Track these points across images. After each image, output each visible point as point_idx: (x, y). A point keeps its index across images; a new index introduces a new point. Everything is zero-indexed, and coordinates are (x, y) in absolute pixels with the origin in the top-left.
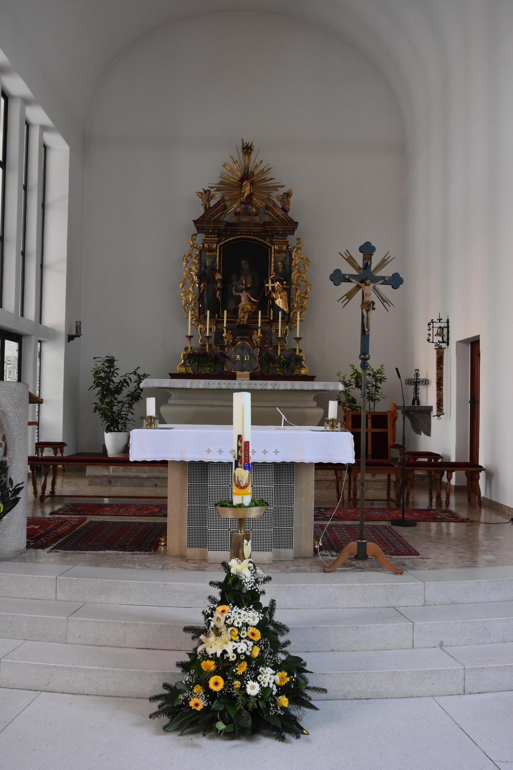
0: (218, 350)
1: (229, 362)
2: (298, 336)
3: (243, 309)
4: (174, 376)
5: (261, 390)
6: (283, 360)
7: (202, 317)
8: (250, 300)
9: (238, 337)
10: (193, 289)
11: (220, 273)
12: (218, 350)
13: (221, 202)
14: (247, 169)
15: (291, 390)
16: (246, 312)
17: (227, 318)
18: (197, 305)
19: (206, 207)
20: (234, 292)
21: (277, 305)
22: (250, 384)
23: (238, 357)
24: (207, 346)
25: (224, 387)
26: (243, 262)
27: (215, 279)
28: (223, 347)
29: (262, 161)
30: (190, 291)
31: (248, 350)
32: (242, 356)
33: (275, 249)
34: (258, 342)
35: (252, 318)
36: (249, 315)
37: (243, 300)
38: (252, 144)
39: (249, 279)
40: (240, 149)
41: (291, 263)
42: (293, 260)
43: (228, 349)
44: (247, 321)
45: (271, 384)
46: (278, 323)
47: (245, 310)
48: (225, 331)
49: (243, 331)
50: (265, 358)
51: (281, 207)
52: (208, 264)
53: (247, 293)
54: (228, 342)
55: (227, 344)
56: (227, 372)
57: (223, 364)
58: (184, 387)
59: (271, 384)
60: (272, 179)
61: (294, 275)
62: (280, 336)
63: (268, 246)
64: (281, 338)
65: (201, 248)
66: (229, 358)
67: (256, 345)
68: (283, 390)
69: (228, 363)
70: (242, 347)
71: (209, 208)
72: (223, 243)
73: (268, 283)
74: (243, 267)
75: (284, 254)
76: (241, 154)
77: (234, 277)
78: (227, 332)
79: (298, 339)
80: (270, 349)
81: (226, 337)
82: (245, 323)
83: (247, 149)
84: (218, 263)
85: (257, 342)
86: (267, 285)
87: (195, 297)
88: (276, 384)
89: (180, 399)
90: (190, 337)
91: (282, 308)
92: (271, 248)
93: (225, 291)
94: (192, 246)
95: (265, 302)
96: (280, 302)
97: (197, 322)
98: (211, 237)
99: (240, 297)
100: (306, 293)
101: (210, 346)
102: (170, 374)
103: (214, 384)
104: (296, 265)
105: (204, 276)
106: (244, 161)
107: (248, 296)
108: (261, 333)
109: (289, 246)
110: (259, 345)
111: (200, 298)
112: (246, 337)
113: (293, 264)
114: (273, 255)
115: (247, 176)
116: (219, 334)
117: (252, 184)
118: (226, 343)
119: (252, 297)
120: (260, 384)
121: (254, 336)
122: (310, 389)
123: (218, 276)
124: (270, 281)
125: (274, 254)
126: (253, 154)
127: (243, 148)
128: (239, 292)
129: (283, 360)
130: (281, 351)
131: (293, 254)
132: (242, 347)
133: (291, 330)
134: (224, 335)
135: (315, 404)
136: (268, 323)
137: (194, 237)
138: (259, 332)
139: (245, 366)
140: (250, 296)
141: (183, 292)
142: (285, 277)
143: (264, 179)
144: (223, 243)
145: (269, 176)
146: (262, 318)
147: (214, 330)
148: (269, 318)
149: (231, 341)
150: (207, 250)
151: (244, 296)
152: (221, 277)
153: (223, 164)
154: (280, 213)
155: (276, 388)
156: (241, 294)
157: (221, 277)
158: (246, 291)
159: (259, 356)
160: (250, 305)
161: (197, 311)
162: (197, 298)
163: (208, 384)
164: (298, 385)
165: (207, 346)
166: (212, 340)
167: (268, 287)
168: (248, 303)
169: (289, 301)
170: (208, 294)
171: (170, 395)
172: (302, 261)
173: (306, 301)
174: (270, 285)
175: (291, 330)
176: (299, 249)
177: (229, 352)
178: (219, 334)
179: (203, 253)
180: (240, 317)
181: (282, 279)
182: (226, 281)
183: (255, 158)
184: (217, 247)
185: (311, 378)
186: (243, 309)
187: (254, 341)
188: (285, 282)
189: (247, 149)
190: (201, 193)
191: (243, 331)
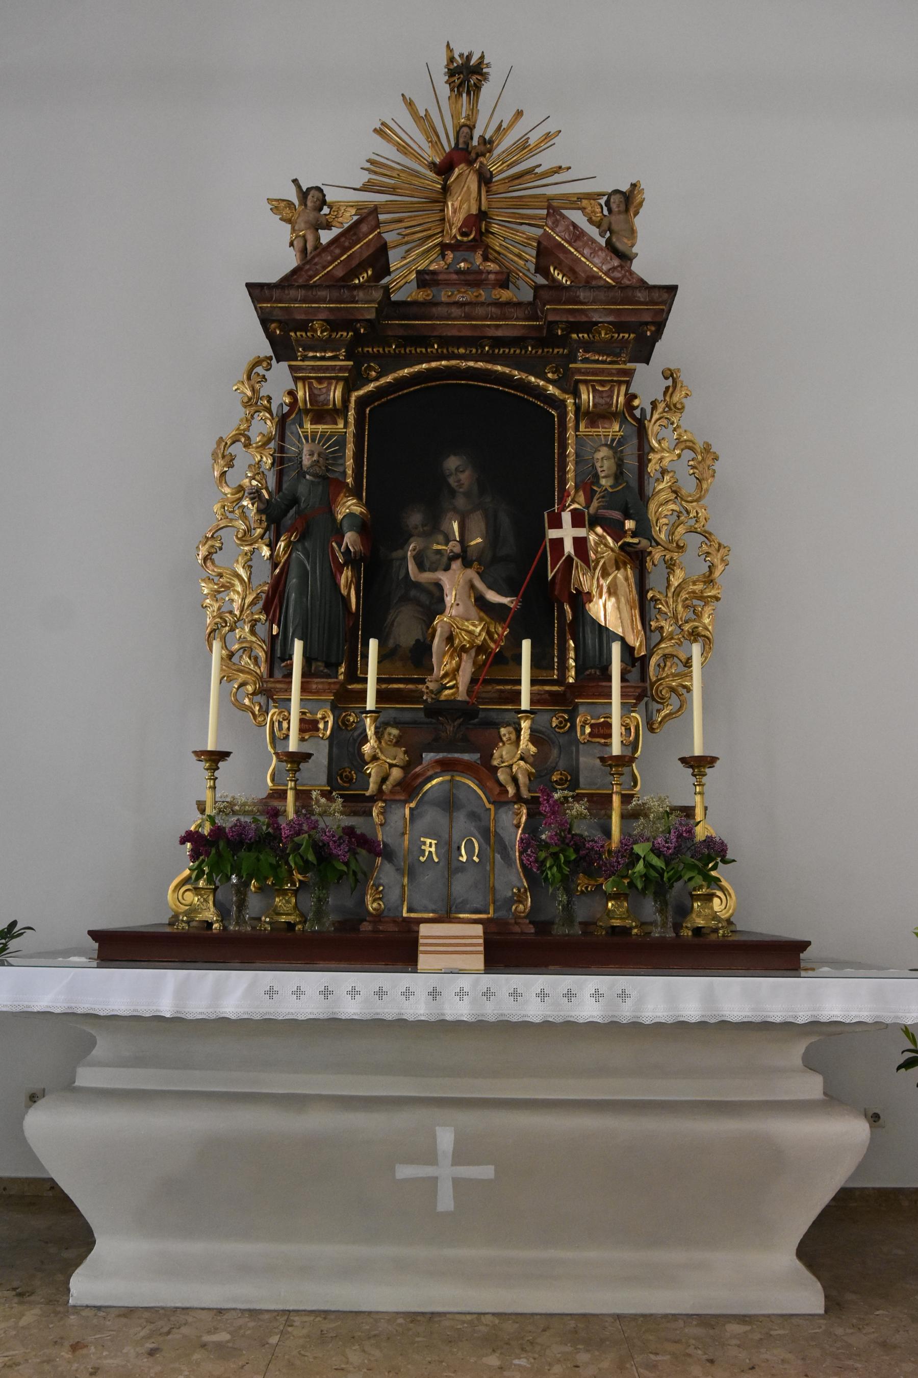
0: (334, 817)
1: (388, 867)
2: (698, 751)
3: (450, 639)
4: (118, 947)
5: (547, 1025)
6: (648, 865)
7: (278, 675)
8: (481, 603)
9: (429, 757)
10: (248, 567)
11: (356, 492)
12: (334, 817)
13: (364, 228)
14: (465, 130)
15: (702, 1025)
16: (463, 649)
17: (379, 681)
18: (261, 629)
19: (304, 250)
20: (412, 567)
21: (594, 622)
22: (488, 994)
23: (430, 846)
24: (290, 795)
25: (351, 1009)
26: (452, 463)
27: (334, 519)
28: (358, 803)
29: (519, 114)
30: (238, 576)
31: (473, 816)
32: (449, 843)
33: (577, 407)
34: (522, 779)
35: (486, 682)
36: (478, 667)
37: (450, 599)
38: (482, 57)
39: (477, 523)
40: (441, 78)
41: (643, 462)
42: (652, 450)
43: (383, 813)
44: (469, 692)
45: (597, 995)
46: (609, 696)
47: (463, 639)
48: (370, 732)
49: (456, 730)
50: (555, 856)
51: (602, 242)
52: (306, 461)
53: (471, 573)
54: (384, 780)
55: (380, 790)
56: (378, 917)
57: (360, 881)
58: (146, 1010)
59: (597, 995)
60: (559, 169)
61: (661, 510)
62: (616, 749)
63: (551, 400)
64: (624, 761)
65: (286, 409)
66: (388, 853)
67: (511, 791)
68: (659, 1028)
69: (386, 874)
70: (449, 803)
71: (316, 248)
72: (371, 386)
73: (558, 524)
74: (452, 481)
75: (616, 427)
76: (444, 90)
77: (415, 519)
78: (379, 734)
79: (699, 765)
80: (579, 808)
81: (375, 758)
82: (462, 696)
83: (466, 75)
84: (350, 463)
85: (515, 779)
86: (553, 534)
87: (257, 598)
88: (623, 995)
89: (138, 1061)
90: (215, 758)
91: (619, 632)
92: (560, 405)
93: (375, 567)
94: (248, 403)
95: (543, 604)
96: (606, 610)
97: (261, 699)
98: (323, 358)
99: (439, 587)
100: (709, 580)
101: (302, 796)
102: (95, 935)
103: (298, 992)
104: (664, 472)
105: (286, 509)
106: (455, 115)
107: (472, 587)
108: (533, 739)
109: (634, 397)
110: (525, 794)
111: (273, 601)
112: (466, 757)
113: (652, 468)
114: (570, 433)
115: (464, 153)
116: (346, 742)
117: (485, 179)
118: (372, 787)
119: (490, 587)
120: (542, 995)
121: (503, 754)
122: (803, 1017)
123: (349, 507)
124: (566, 517)
125: (577, 429)
126: (488, 91)
127: (451, 73)
128: (434, 570)
129: (648, 865)
130: (623, 817)
131: (652, 428)
132: (449, 803)
133: (652, 730)
134: (367, 748)
135: (812, 1087)
136: (555, 699)
137: (260, 370)
138: (525, 734)
139: (461, 886)
140: (480, 585)
141: (209, 580)
142: (624, 503)
143: (530, 171)
144: (371, 386)
145: (545, 160)
146: (533, 682)
147: (327, 723)
148: (561, 681)
149: (396, 773)
150: (307, 411)
151: (454, 585)
152: (357, 510)
153: (378, 126)
154: (598, 265)
155: (625, 1013)
156: (445, 579)
157: (357, 510)
158: (467, 564)
159: (525, 845)
160: (481, 620)
161: (262, 655)
162: (260, 604)
163: (271, 992)
164: (736, 996)
165: (290, 795)
166: (316, 772)
167: (559, 542)
168: (474, 612)
169: (644, 606)
170: (304, 576)
171: (93, 1043)
172: (688, 454)
173: (708, 610)
174: (567, 533)
175: (652, 730)
176: (673, 408)
177: (388, 824)
178: (346, 742)
179: (293, 429)
180: (439, 671)
181: (616, 515)
182: (383, 533)
183: (490, 110)
184: (345, 400)
185: (781, 956)
186: (450, 639)
187: (502, 776)
188: (629, 524)
189: (466, 75)
190: (290, 204)
191: (456, 730)
